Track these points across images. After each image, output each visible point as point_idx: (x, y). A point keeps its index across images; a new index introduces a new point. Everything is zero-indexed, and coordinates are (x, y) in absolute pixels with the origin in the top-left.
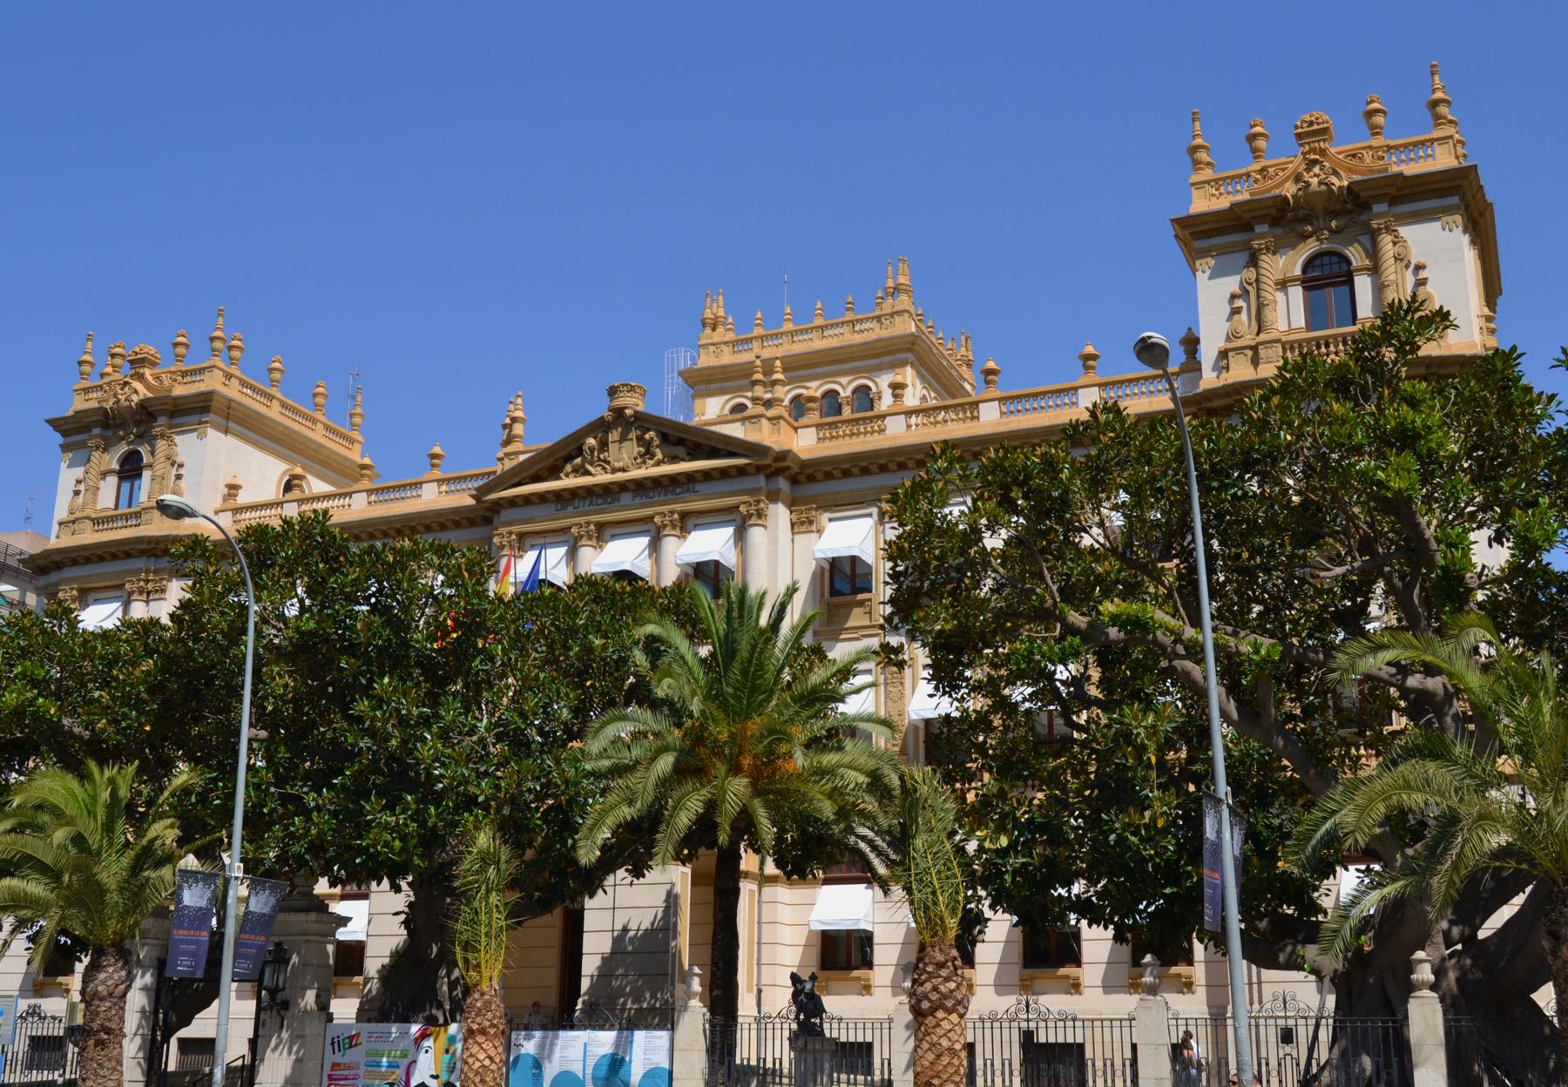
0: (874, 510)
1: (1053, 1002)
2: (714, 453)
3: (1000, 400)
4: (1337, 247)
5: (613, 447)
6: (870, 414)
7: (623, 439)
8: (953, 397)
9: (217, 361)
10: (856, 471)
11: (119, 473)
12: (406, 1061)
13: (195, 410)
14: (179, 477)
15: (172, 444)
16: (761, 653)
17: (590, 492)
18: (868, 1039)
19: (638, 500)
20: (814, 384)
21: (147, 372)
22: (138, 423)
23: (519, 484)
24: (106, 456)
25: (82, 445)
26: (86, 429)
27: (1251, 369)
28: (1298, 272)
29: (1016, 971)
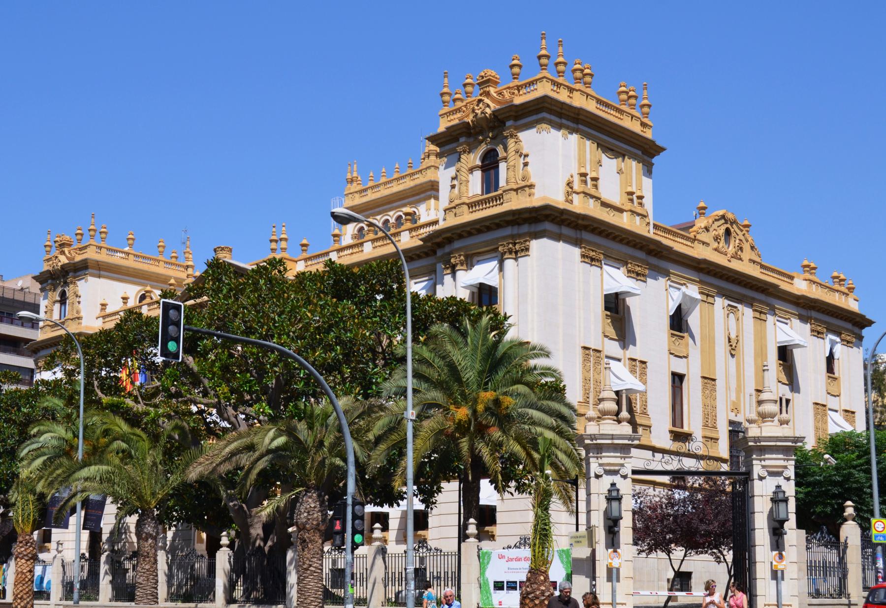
6: (415, 225)
9: (92, 242)
11: (60, 301)
13: (80, 269)
14: (526, 164)
21: (492, 90)
22: (492, 129)
24: (472, 156)
25: (453, 151)
28: (479, 163)
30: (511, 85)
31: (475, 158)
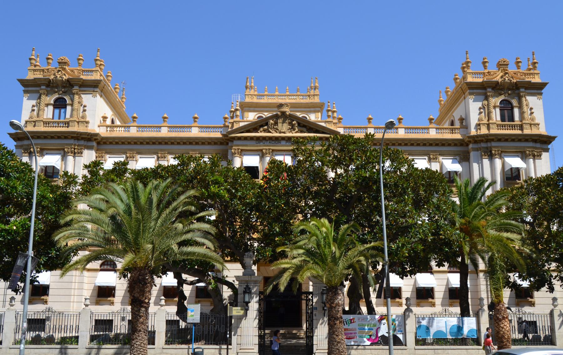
0: (155, 156)
1: (527, 309)
2: (310, 130)
3: (375, 128)
4: (509, 99)
5: (280, 125)
7: (283, 122)
8: (125, 123)
10: (182, 143)
12: (376, 328)
13: (93, 86)
14: (84, 111)
15: (80, 97)
16: (496, 200)
17: (270, 138)
18: (535, 320)
19: (288, 144)
20: (266, 114)
21: (67, 68)
23: (242, 132)
26: (39, 86)
27: (530, 130)
28: (52, 102)
29: (95, 298)
30: (78, 68)
31: (50, 100)
